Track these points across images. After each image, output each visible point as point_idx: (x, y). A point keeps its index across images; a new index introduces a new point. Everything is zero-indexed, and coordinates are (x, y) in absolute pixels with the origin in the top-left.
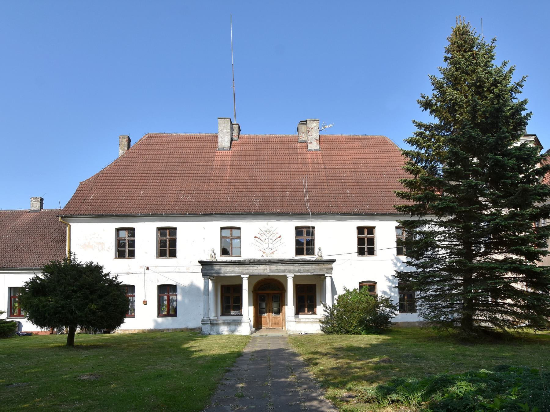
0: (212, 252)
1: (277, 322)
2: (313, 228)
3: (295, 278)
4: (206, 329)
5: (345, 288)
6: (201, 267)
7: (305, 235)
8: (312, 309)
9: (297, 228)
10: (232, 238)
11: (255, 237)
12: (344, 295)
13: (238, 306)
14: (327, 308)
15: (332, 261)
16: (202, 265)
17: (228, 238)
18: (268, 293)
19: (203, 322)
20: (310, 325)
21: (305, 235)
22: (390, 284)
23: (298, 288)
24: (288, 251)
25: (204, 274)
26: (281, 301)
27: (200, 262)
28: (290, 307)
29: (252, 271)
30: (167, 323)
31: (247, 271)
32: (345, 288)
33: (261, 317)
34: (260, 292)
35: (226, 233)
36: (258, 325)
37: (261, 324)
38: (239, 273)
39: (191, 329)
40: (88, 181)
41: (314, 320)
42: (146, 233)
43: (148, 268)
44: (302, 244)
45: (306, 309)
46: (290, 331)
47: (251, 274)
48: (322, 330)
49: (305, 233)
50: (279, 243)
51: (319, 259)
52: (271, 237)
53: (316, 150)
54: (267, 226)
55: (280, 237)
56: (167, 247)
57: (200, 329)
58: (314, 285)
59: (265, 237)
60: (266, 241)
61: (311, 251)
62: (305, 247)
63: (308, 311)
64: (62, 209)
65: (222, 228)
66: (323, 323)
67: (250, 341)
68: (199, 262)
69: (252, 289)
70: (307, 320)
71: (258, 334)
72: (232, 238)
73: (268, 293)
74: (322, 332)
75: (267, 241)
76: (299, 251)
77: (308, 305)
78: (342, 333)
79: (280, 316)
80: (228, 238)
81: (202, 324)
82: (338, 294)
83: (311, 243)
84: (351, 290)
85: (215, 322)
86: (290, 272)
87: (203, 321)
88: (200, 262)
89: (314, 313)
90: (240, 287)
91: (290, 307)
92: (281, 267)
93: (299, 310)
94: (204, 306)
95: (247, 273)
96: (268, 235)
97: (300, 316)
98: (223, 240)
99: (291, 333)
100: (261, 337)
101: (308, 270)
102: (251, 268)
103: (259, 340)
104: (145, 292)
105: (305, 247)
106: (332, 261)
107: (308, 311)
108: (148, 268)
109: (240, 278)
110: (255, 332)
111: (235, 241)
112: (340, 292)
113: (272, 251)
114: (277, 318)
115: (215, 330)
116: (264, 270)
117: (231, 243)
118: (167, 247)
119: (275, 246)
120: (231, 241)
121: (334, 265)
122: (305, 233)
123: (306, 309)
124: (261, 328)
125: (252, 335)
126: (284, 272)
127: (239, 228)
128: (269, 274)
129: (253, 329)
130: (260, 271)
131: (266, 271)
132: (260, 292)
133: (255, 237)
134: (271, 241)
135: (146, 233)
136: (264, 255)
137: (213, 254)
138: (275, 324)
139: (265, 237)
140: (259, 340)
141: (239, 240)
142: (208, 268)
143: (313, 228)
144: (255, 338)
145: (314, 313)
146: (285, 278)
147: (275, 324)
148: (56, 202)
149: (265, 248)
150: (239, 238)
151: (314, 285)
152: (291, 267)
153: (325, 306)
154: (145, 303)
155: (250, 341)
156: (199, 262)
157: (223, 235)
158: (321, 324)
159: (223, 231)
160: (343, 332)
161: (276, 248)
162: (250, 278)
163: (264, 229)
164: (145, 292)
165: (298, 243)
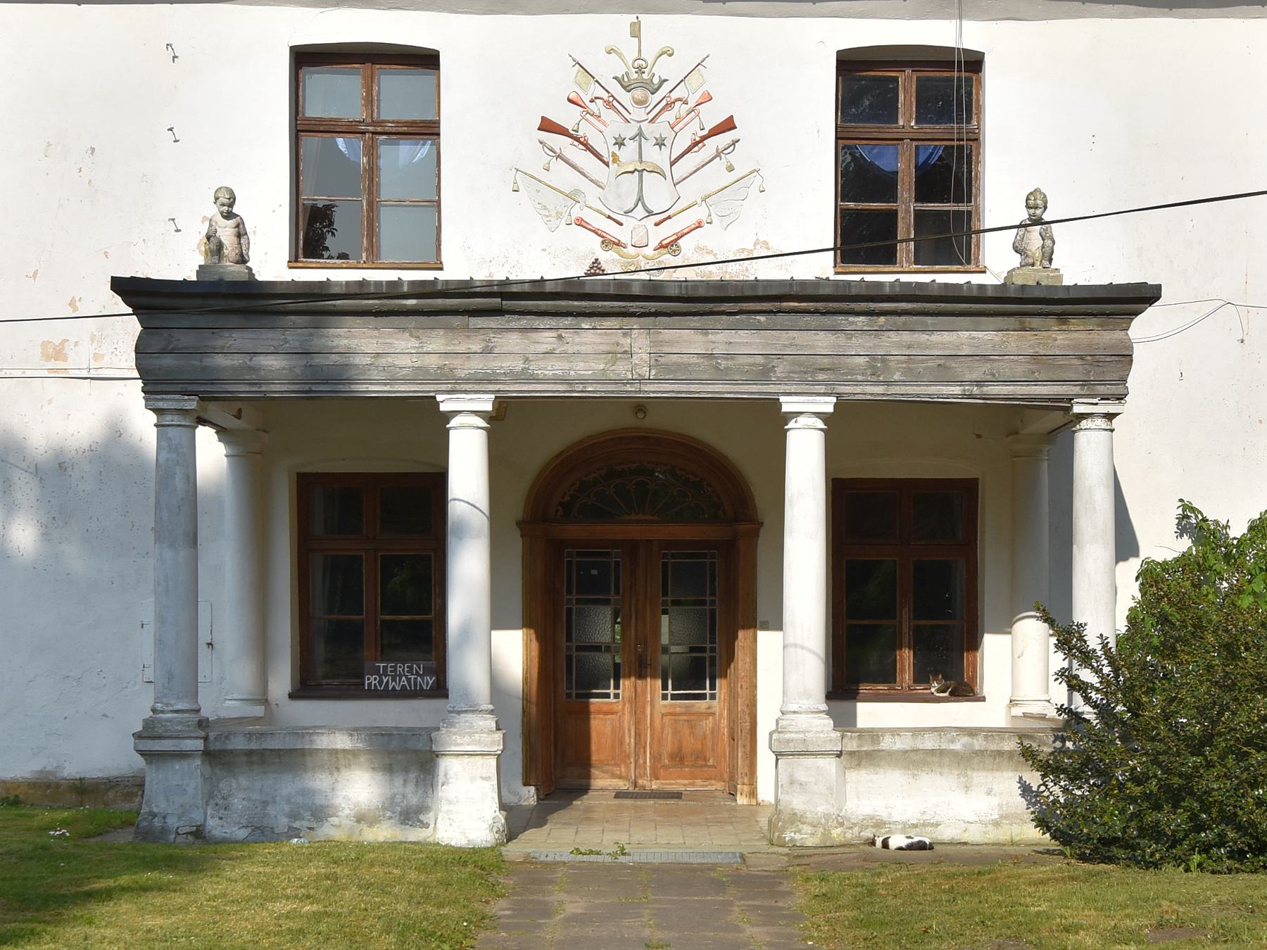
0: (213, 211)
1: (690, 744)
2: (974, 63)
3: (841, 428)
4: (176, 795)
5: (1187, 510)
6: (133, 327)
7: (906, 118)
8: (948, 665)
9: (851, 65)
10: (375, 132)
12: (1183, 561)
13: (416, 631)
14: (1086, 657)
16: (138, 310)
17: (351, 129)
18: (641, 533)
19: (152, 740)
20: (942, 776)
21: (906, 118)
23: (856, 508)
24: (786, 220)
25: (155, 385)
26: (728, 595)
27: (125, 287)
28: (788, 654)
29: (518, 365)
31: (477, 365)
32: (1187, 510)
33: (584, 714)
34: (574, 531)
35: (336, 94)
36: (553, 759)
37: (582, 763)
38: (420, 374)
39: (84, 790)
41: (978, 743)
44: (885, 185)
45: (906, 657)
46: (796, 819)
47: (515, 389)
48: (1042, 822)
49: (906, 100)
50: (715, 175)
51: (1028, 278)
52: (661, 128)
54: (629, 48)
57: (133, 787)
58: (969, 488)
59: (614, 125)
61: (951, 237)
62: (906, 206)
63: (922, 676)
65: (306, 58)
66: (1050, 769)
67: (500, 907)
68: (120, 286)
69: (516, 510)
70: (929, 743)
71: (555, 841)
72: (375, 132)
73: (641, 533)
74: (1033, 833)
75: (628, 153)
76: (861, 236)
77: (917, 630)
78: (1206, 849)
79: (715, 704)
80: (351, 129)
81: (147, 755)
82: (1144, 554)
83: (950, 176)
84: (1238, 530)
85: (238, 743)
86: (808, 375)
87: (149, 731)
88: (125, 287)
89: (963, 688)
90: (433, 485)
91: (788, 654)
92: (740, 342)
93: (854, 667)
94: (161, 619)
95: (479, 381)
96: (639, 113)
97: (869, 714)
98: (311, 143)
99: (806, 836)
100: (586, 874)
101: (944, 368)
102: (513, 342)
103: (574, 905)
105: (906, 206)
106: (1139, 297)
107: (922, 676)
109: (427, 422)
110: (537, 817)
111: (400, 157)
112: (1162, 543)
113: (668, 231)
114: (693, 720)
115: (237, 802)
116: (614, 355)
117: (372, 171)
119: (690, 191)
120: (371, 152)
121: (1142, 327)
122: (906, 100)
123: (906, 657)
124: (584, 789)
125: (514, 850)
126: (764, 374)
127: (427, 60)
128: (652, 390)
129: (529, 796)
130: (582, 368)
131: (621, 369)
132: (574, 531)
133: (547, 126)
134: (658, 157)
137: (226, 233)
138: (679, 758)
139: (614, 125)
140: (574, 905)
141: (424, 150)
142: (185, 339)
143: (974, 63)
144: (537, 874)
145: (963, 688)
146: (770, 423)
147: (679, 758)
149: (616, 208)
150: (428, 130)
151: (969, 488)
152: (818, 341)
153: (1069, 638)
155: (500, 907)
156: (120, 286)
157: (314, 110)
158: (1034, 779)
159: (318, 80)
160: (1221, 841)
161: (699, 213)
162: (506, 420)
163: (608, 69)
165: (858, 179)
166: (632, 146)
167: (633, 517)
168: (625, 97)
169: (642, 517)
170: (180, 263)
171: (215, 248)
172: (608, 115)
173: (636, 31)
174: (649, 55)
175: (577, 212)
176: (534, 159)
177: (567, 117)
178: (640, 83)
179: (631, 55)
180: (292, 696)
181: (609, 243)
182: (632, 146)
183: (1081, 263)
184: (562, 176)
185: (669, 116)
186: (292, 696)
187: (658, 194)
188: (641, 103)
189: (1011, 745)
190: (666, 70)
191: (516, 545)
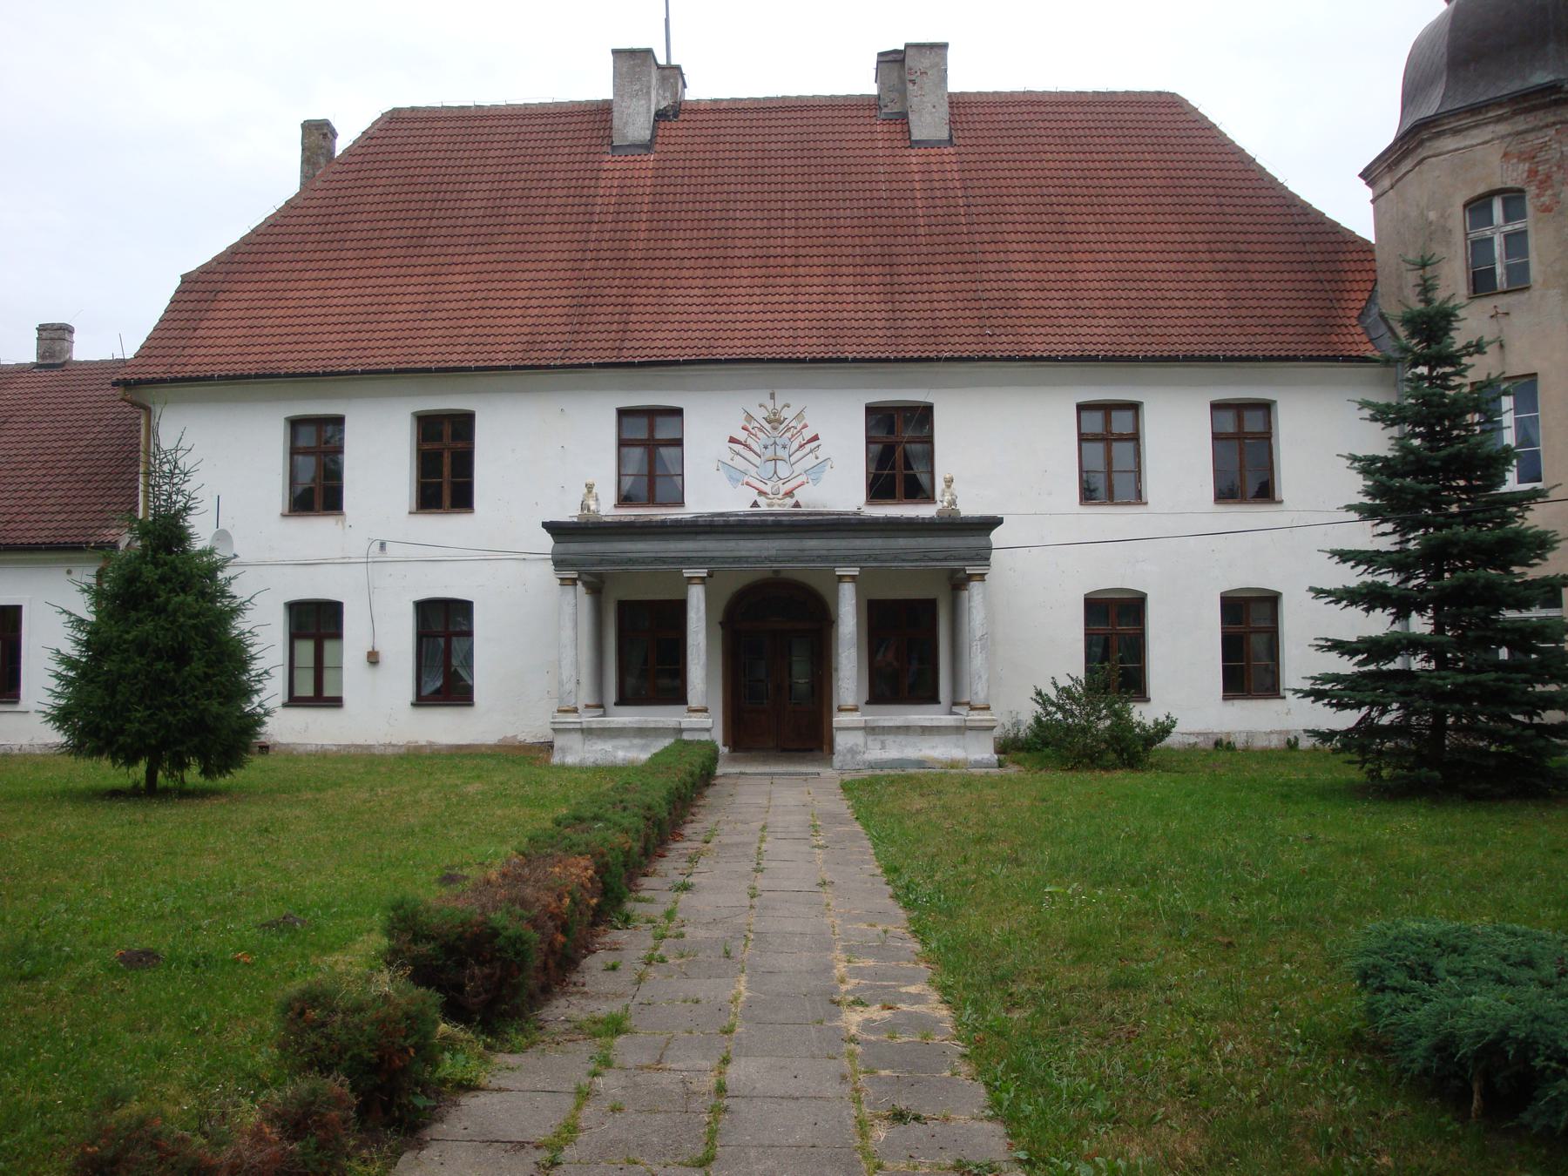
11: (732, 440)
15: (991, 523)
22: (61, 669)
24: (838, 481)
30: (444, 727)
40: (205, 270)
42: (380, 451)
43: (383, 546)
50: (810, 461)
53: (937, 144)
54: (770, 404)
55: (816, 438)
56: (445, 477)
60: (773, 455)
64: (128, 357)
69: (719, 616)
104: (667, 21)
106: (991, 523)
108: (383, 546)
118: (445, 477)
119: (798, 468)
121: (997, 536)
127: (678, 412)
133: (732, 440)
135: (380, 451)
136: (762, 501)
148: (114, 331)
150: (678, 443)
154: (373, 658)
164: (667, 21)
166: (771, 449)
167: (142, 439)
168: (768, 426)
169: (143, 431)
170: (568, 513)
171: (584, 506)
172: (760, 435)
173: (772, 396)
174: (779, 407)
175: (746, 479)
176: (727, 456)
177: (742, 436)
178: (775, 421)
179: (770, 408)
180: (285, 705)
181: (761, 493)
182: (771, 449)
183: (969, 508)
184: (739, 462)
185: (788, 435)
186: (285, 705)
187: (783, 469)
188: (775, 429)
189: (306, 649)
190: (786, 413)
191: (719, 632)
